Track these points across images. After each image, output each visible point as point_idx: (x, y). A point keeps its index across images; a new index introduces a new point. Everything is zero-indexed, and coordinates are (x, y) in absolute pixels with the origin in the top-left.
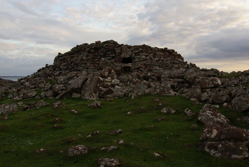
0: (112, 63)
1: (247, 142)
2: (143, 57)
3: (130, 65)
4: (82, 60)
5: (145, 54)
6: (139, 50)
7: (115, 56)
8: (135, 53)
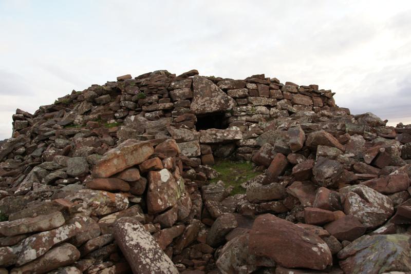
0: (163, 129)
1: (245, 195)
2: (259, 108)
3: (237, 132)
4: (71, 124)
5: (265, 100)
6: (246, 87)
7: (172, 108)
8: (235, 98)
